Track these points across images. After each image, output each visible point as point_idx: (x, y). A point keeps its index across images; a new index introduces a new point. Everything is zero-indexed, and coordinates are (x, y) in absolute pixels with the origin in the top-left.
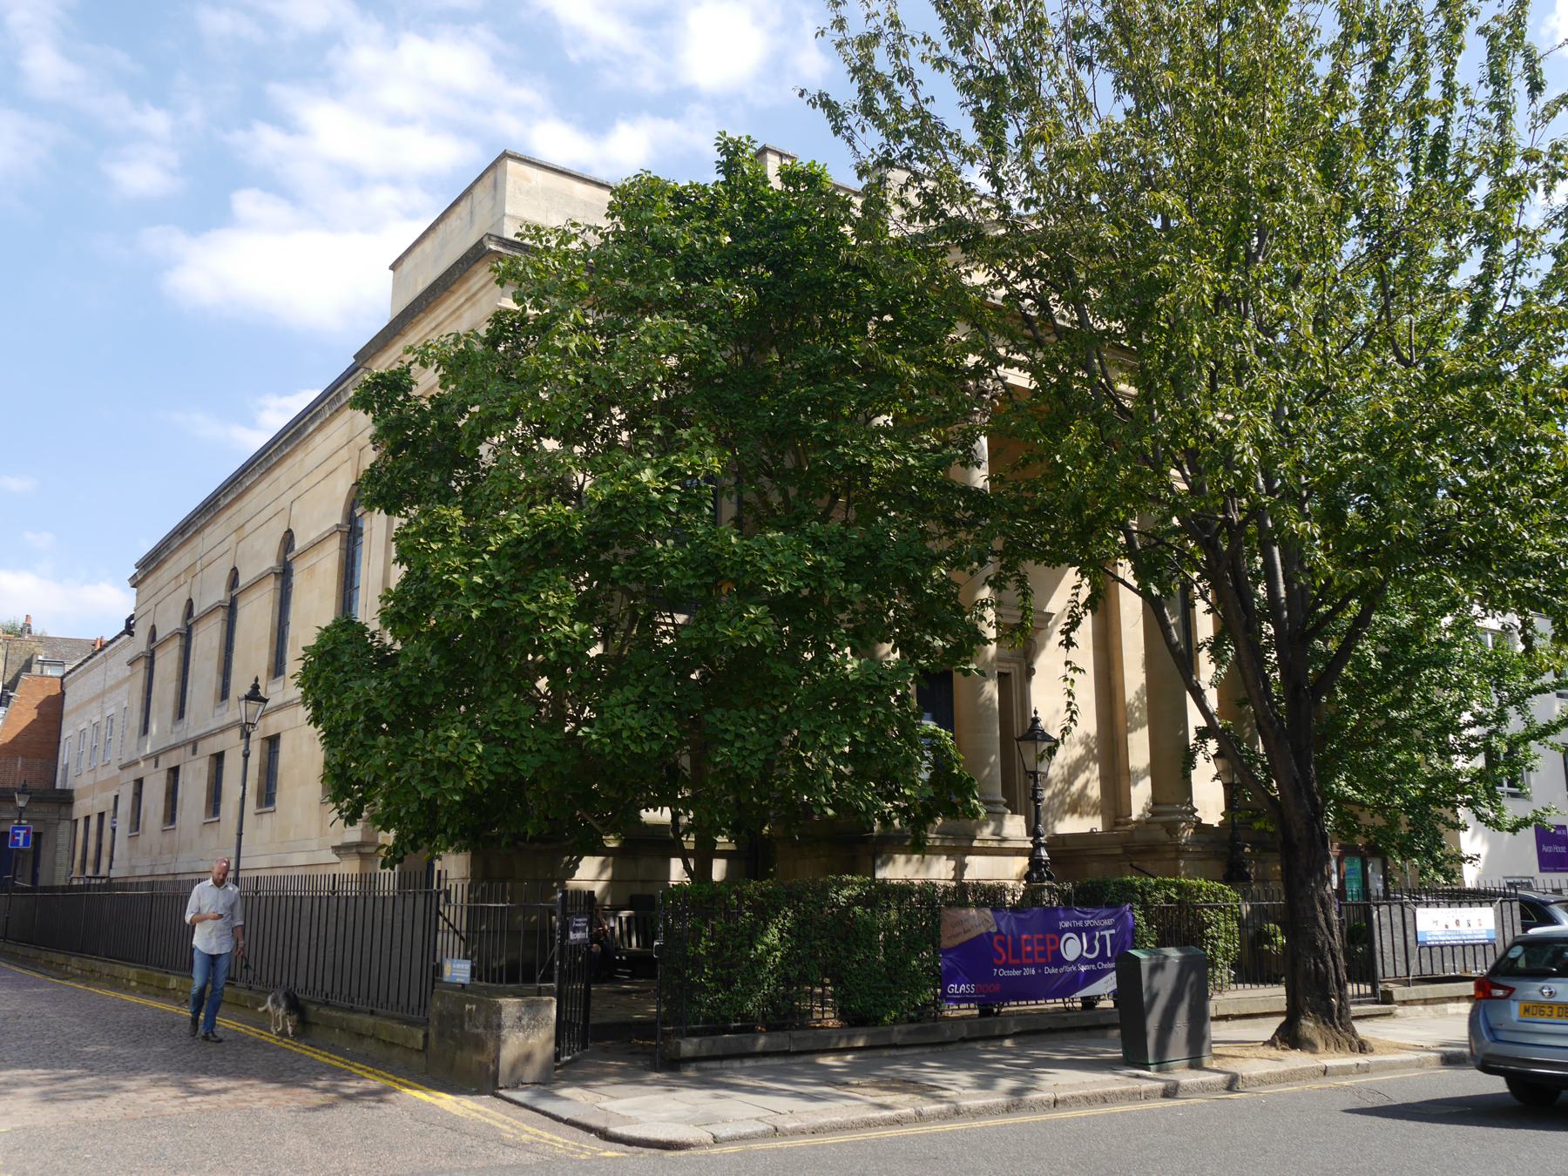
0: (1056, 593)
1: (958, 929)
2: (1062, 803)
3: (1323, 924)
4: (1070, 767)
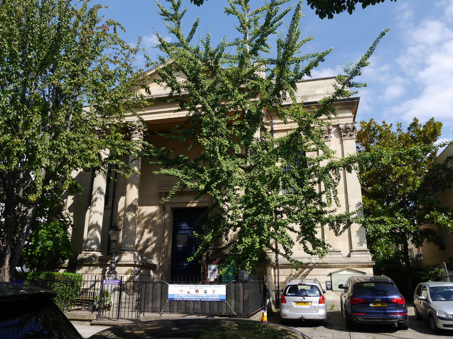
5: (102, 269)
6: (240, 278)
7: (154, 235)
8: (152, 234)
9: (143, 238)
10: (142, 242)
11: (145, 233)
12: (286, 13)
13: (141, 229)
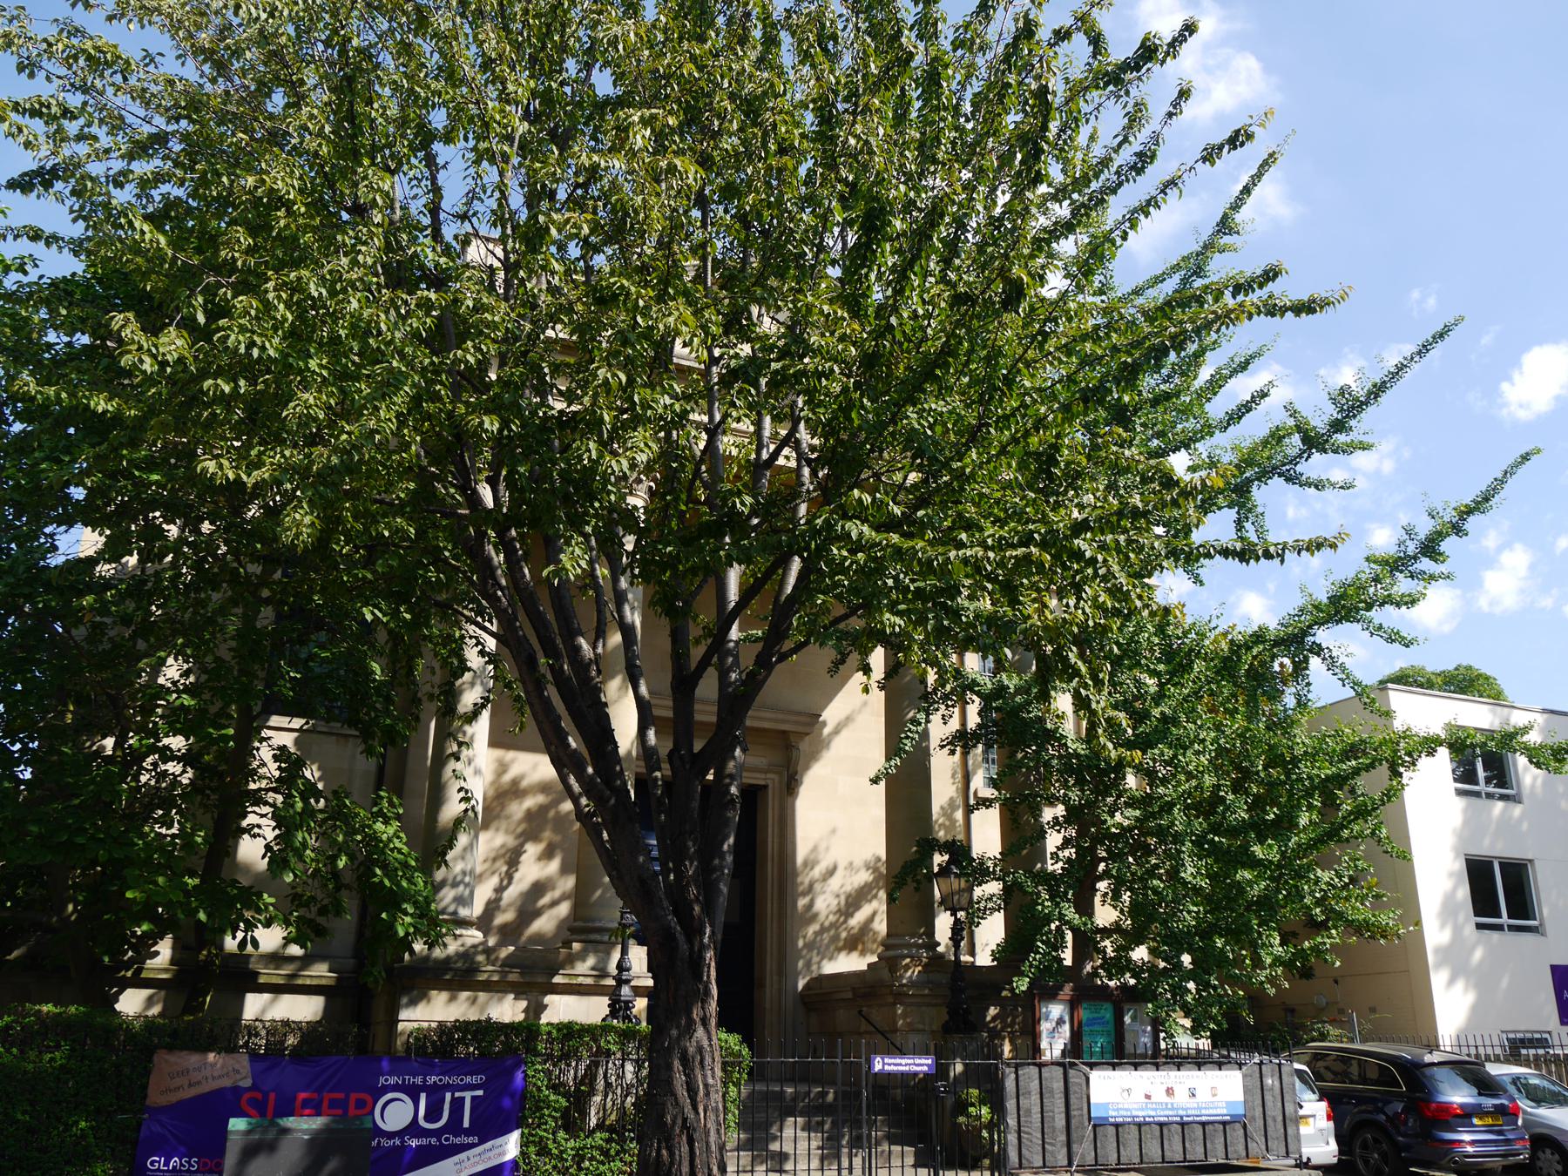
0: (840, 694)
1: (178, 1081)
2: (836, 938)
3: (682, 1092)
4: (848, 897)
5: (523, 1004)
6: (1129, 1048)
7: (564, 870)
8: (554, 866)
9: (517, 876)
10: (511, 893)
11: (524, 858)
12: (1175, 104)
13: (511, 841)
